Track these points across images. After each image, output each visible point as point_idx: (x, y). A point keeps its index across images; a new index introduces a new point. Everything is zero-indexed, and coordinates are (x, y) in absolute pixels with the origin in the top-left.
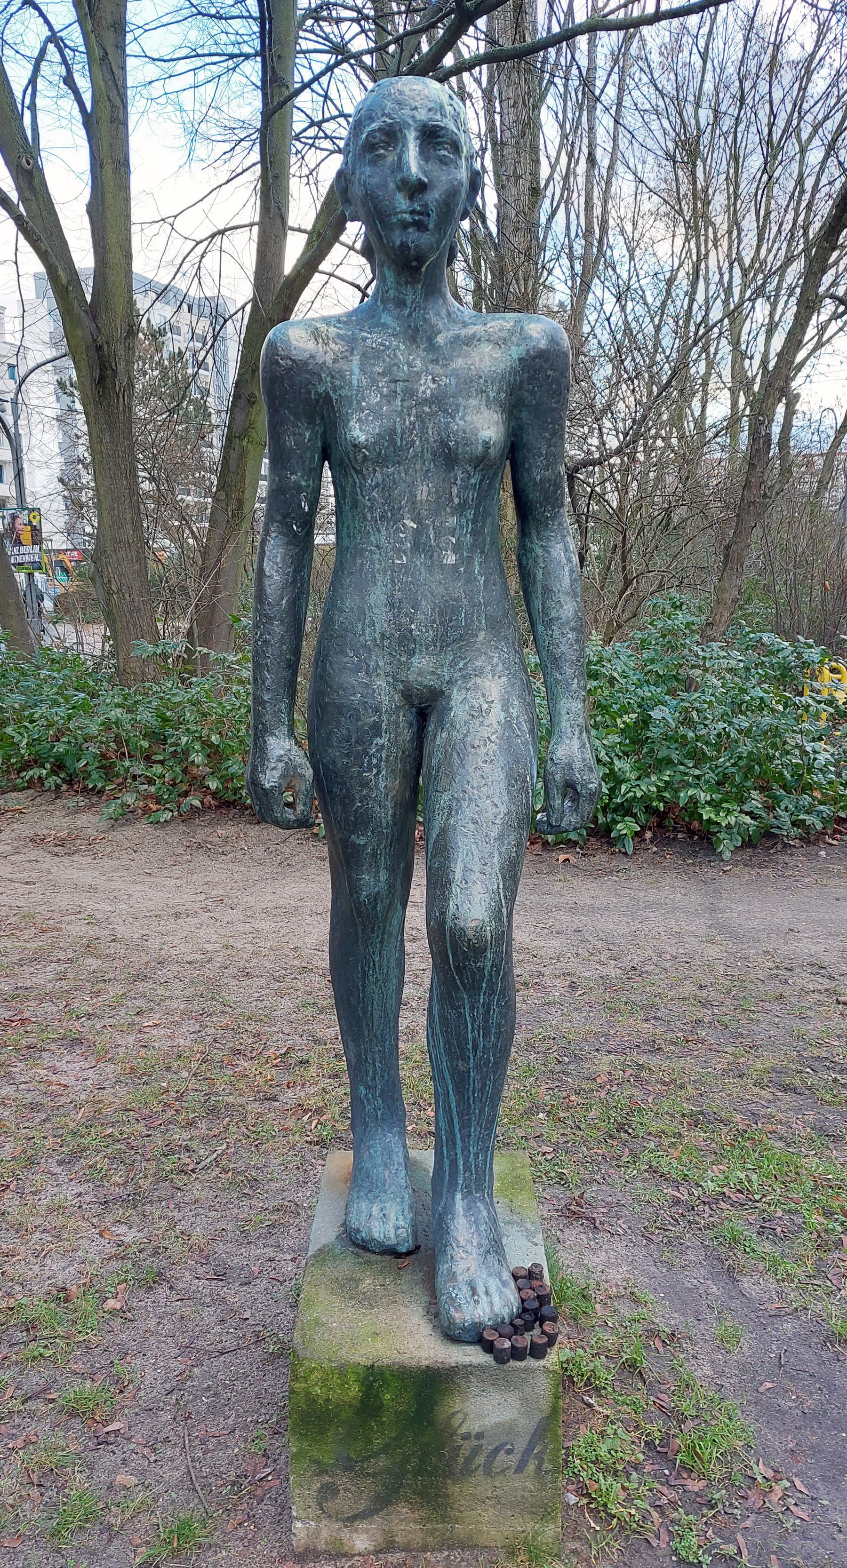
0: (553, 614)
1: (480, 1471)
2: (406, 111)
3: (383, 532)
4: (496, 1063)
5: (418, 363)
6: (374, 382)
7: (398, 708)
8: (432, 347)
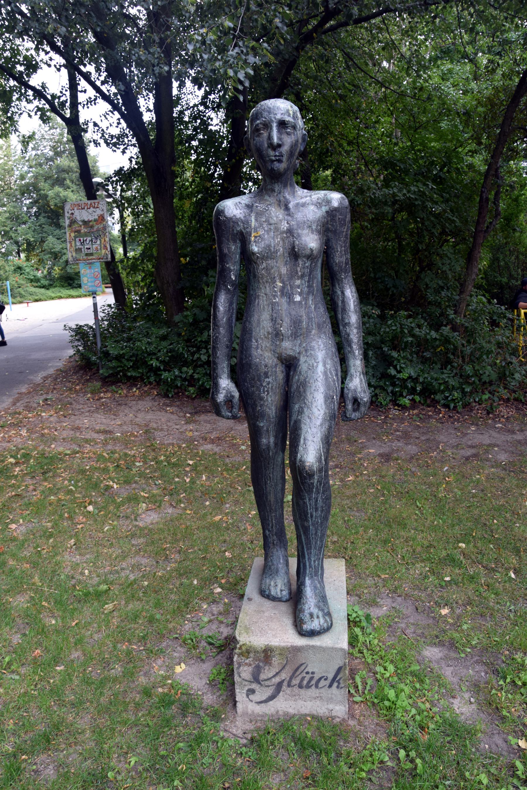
0: (347, 321)
1: (313, 687)
2: (272, 115)
4: (322, 523)
5: (281, 216)
6: (261, 225)
7: (276, 365)
8: (287, 208)
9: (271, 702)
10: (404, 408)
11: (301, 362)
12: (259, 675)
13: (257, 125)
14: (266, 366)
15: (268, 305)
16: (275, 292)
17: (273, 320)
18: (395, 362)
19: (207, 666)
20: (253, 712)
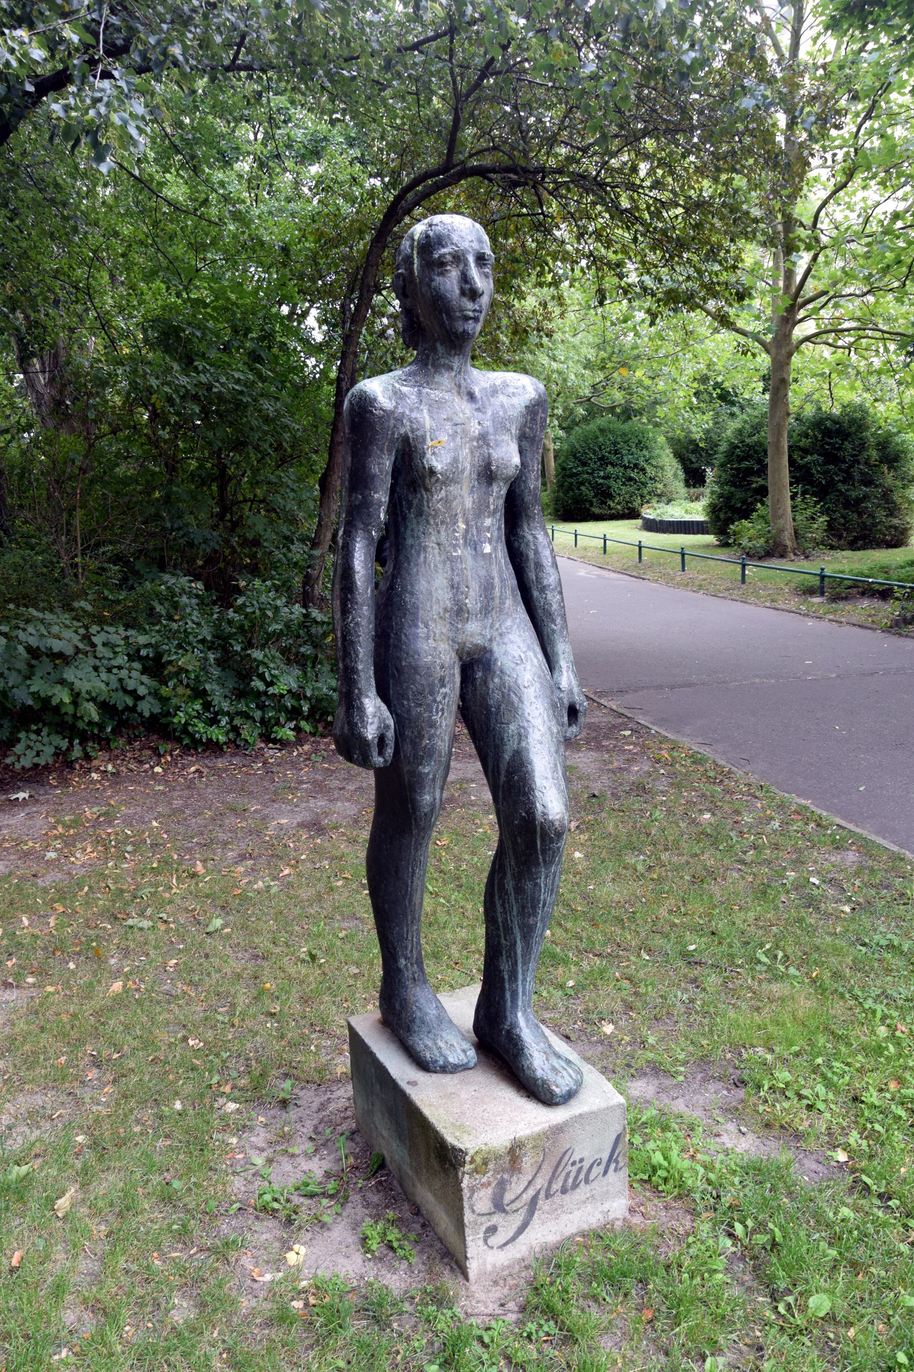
3: (443, 533)
9: (521, 1237)
10: (283, 744)
11: (496, 655)
12: (502, 1196)
13: (444, 255)
14: (442, 667)
15: (444, 563)
16: (457, 539)
17: (454, 587)
18: (261, 669)
19: (340, 1233)
20: (494, 1266)
